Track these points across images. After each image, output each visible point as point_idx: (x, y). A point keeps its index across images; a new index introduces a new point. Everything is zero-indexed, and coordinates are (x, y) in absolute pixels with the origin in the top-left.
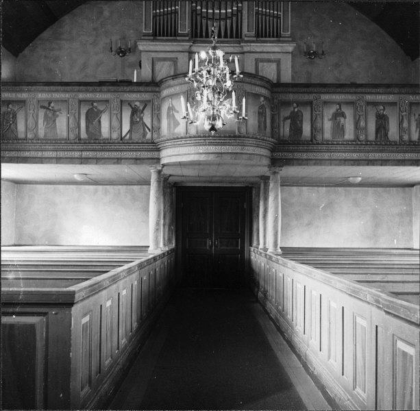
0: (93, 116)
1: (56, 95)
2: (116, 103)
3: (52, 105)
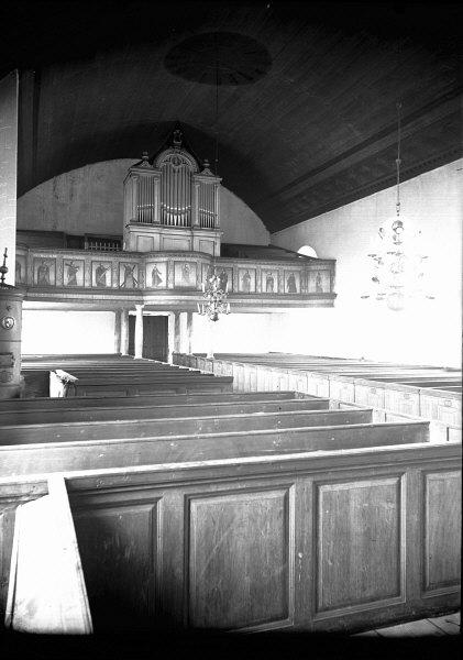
0: (100, 271)
2: (116, 265)
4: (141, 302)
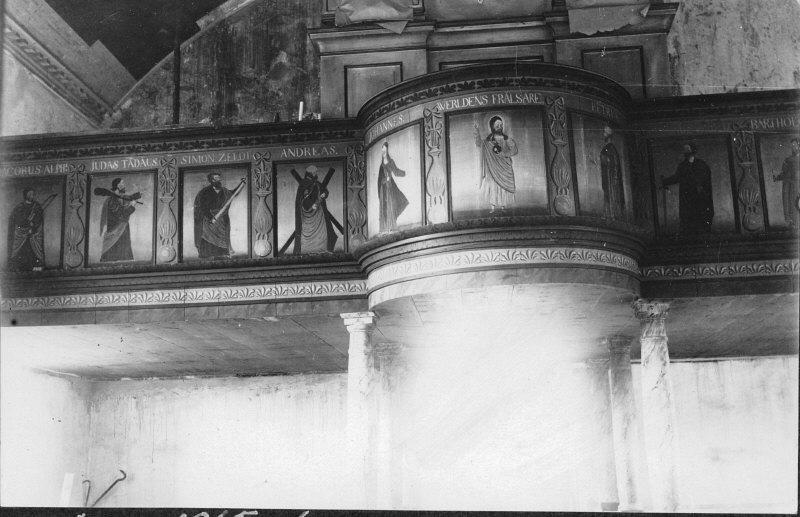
0: (212, 203)
1: (112, 167)
2: (262, 172)
3: (121, 184)
4: (360, 302)
